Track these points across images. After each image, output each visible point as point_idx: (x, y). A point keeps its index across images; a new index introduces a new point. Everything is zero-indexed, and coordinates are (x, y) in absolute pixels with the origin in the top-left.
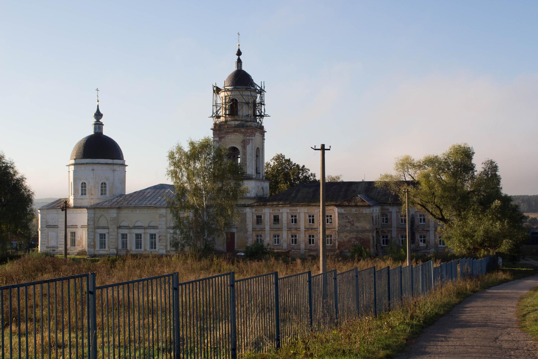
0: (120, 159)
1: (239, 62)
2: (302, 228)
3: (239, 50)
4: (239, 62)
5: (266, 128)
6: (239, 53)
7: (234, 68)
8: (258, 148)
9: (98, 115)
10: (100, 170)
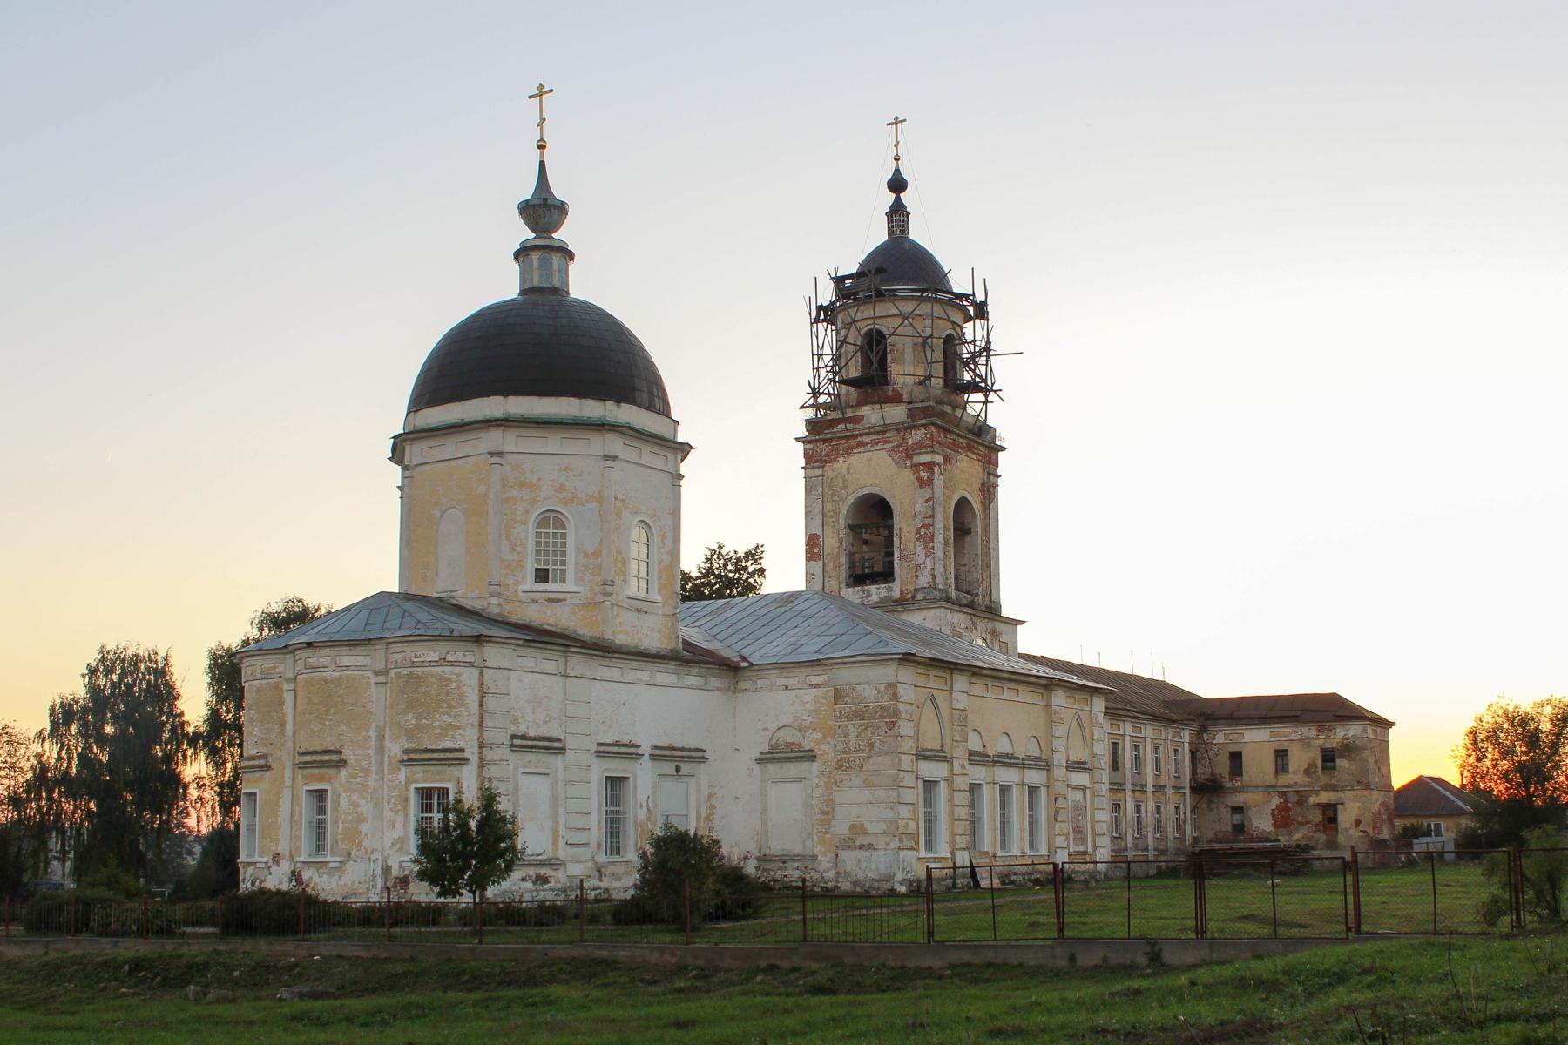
0: (650, 407)
1: (898, 213)
2: (1129, 794)
3: (897, 171)
4: (898, 213)
5: (1004, 436)
6: (897, 184)
7: (879, 235)
8: (962, 506)
9: (543, 211)
10: (543, 458)
